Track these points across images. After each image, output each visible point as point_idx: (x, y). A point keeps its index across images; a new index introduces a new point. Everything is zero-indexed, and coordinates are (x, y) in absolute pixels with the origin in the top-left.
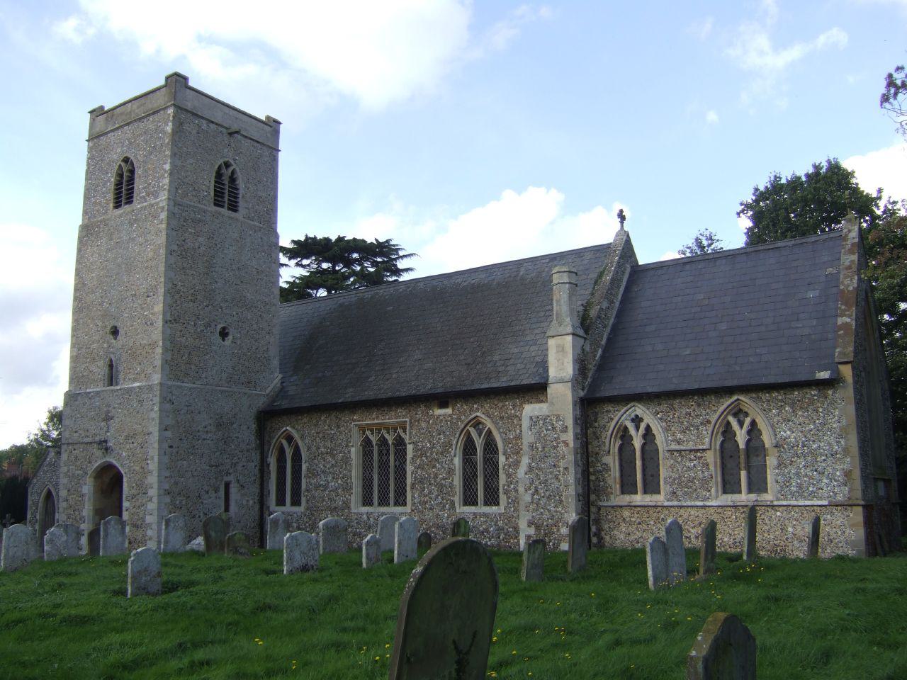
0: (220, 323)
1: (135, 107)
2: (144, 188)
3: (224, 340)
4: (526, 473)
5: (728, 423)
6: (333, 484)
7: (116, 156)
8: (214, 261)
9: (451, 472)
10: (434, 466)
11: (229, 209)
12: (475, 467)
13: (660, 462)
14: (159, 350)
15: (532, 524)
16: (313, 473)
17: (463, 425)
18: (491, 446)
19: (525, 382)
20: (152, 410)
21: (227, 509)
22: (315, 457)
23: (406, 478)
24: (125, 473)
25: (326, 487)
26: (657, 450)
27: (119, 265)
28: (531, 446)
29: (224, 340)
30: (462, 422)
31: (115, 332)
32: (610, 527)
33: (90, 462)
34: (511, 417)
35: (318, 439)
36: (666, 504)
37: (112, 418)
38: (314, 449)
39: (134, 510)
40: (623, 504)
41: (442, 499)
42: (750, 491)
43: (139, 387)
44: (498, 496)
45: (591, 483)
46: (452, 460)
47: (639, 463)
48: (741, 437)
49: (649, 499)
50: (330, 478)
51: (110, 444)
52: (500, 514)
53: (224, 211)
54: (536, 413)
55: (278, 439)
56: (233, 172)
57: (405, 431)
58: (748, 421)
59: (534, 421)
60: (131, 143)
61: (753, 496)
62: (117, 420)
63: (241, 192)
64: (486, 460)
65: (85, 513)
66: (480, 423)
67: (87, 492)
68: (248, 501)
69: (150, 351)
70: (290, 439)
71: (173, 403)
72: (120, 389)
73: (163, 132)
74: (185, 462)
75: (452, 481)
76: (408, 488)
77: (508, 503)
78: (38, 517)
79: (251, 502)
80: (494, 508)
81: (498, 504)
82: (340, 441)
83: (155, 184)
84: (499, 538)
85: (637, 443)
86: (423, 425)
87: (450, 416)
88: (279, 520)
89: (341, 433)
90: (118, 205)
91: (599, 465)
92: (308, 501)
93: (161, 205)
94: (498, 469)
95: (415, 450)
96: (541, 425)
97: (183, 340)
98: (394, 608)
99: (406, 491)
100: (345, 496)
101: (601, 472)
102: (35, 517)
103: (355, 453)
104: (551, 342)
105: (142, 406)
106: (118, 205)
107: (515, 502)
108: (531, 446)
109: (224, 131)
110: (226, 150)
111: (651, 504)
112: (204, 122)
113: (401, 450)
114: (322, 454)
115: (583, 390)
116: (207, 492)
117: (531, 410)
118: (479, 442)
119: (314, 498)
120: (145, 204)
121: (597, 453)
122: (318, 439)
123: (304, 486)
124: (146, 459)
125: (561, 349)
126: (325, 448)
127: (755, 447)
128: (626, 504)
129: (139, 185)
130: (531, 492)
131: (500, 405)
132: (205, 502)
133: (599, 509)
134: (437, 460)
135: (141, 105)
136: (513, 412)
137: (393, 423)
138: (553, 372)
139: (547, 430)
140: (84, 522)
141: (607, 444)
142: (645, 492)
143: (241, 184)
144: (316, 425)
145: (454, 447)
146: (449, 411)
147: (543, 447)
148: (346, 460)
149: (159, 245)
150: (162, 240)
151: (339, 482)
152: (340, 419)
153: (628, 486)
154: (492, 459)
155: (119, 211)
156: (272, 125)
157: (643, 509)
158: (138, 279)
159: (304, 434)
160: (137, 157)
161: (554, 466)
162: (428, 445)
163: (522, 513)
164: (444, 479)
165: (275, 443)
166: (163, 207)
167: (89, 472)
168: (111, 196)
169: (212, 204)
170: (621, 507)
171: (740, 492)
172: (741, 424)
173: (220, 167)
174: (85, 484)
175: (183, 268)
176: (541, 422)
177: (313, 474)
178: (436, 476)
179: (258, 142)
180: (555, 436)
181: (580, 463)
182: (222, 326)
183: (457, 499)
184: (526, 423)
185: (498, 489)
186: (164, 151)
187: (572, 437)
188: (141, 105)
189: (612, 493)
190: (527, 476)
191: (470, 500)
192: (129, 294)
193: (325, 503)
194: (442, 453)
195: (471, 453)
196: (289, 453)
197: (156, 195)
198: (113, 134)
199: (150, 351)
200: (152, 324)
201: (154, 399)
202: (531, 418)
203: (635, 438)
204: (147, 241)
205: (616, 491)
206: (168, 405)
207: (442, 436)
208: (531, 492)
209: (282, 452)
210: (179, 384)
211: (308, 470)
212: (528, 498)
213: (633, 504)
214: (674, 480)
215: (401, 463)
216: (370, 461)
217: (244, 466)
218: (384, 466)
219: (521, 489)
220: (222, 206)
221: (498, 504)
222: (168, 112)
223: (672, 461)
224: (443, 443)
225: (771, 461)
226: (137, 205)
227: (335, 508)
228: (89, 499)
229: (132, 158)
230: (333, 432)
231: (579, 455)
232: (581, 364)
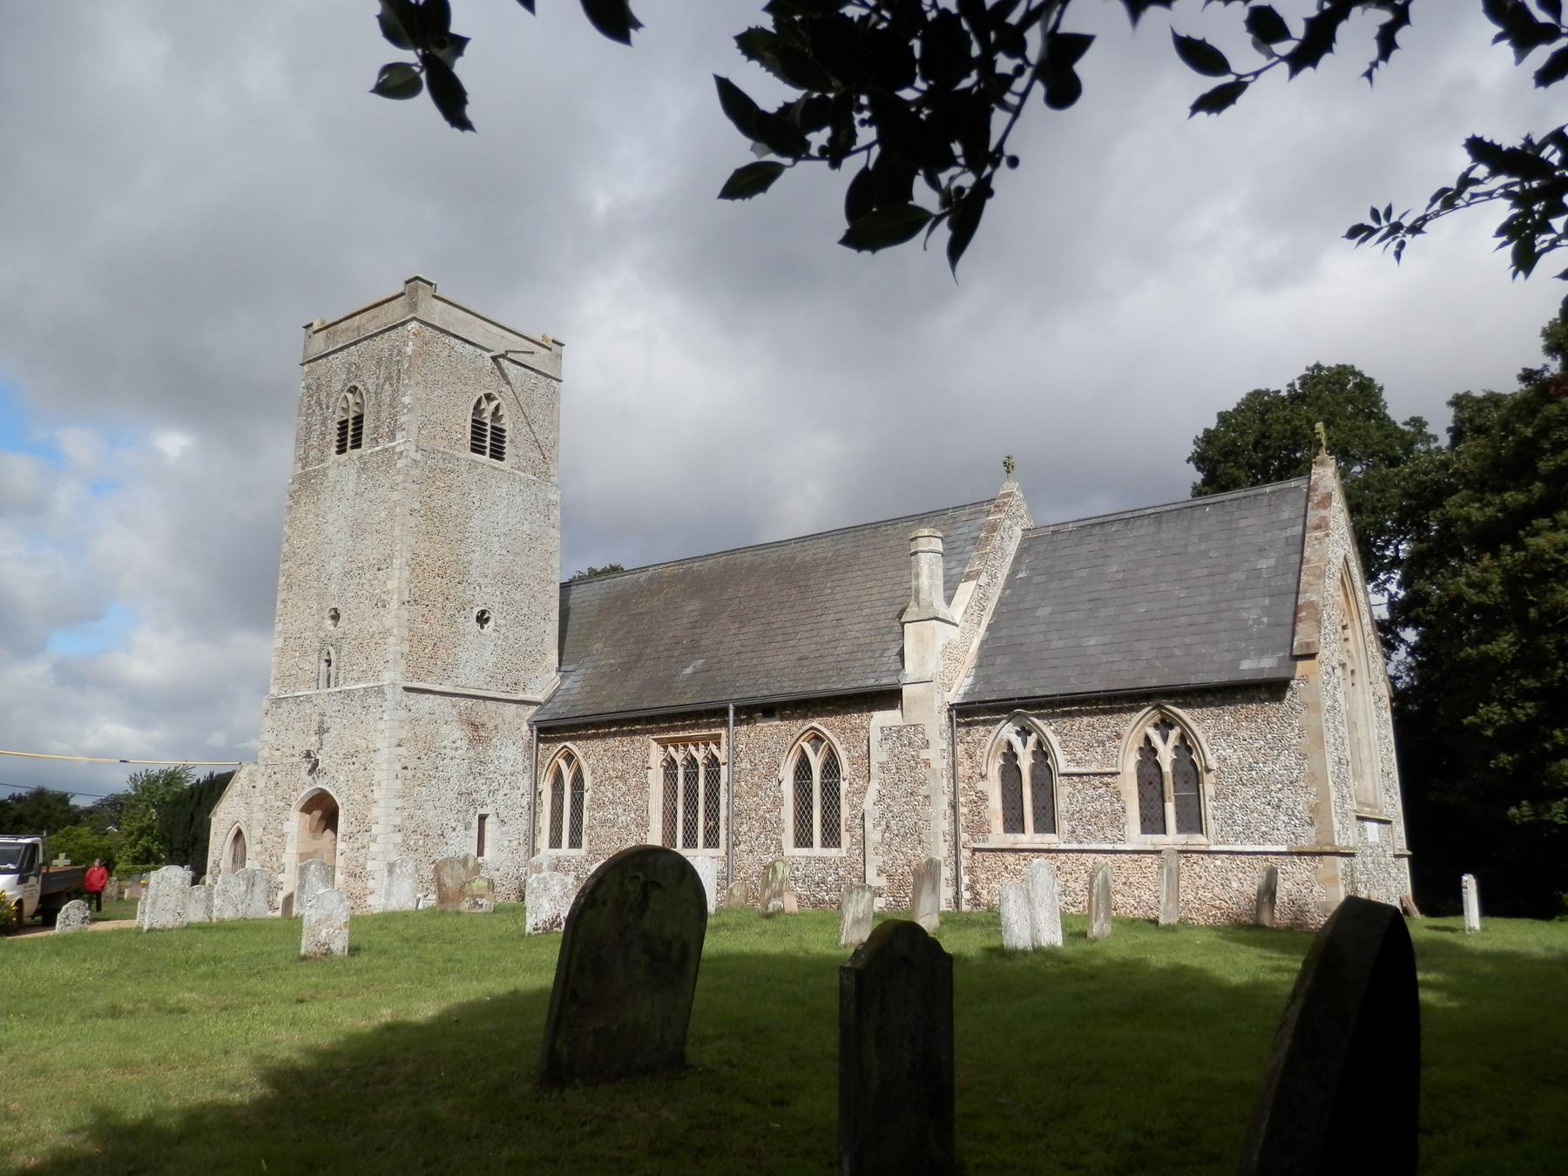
1: (364, 321)
5: (1147, 739)
6: (624, 818)
9: (778, 803)
28: (883, 767)
31: (336, 617)
48: (1166, 755)
53: (485, 459)
58: (1032, 739)
61: (1183, 838)
83: (390, 423)
85: (1025, 762)
90: (341, 450)
94: (839, 798)
97: (426, 626)
103: (656, 778)
106: (339, 453)
108: (883, 767)
117: (881, 719)
118: (816, 763)
127: (1190, 772)
148: (643, 786)
155: (344, 456)
159: (590, 754)
171: (1164, 832)
172: (1165, 738)
173: (479, 402)
179: (532, 369)
183: (788, 836)
184: (875, 736)
191: (803, 839)
209: (558, 777)
213: (1018, 846)
218: (691, 778)
219: (869, 825)
225: (1209, 788)
230: (625, 749)
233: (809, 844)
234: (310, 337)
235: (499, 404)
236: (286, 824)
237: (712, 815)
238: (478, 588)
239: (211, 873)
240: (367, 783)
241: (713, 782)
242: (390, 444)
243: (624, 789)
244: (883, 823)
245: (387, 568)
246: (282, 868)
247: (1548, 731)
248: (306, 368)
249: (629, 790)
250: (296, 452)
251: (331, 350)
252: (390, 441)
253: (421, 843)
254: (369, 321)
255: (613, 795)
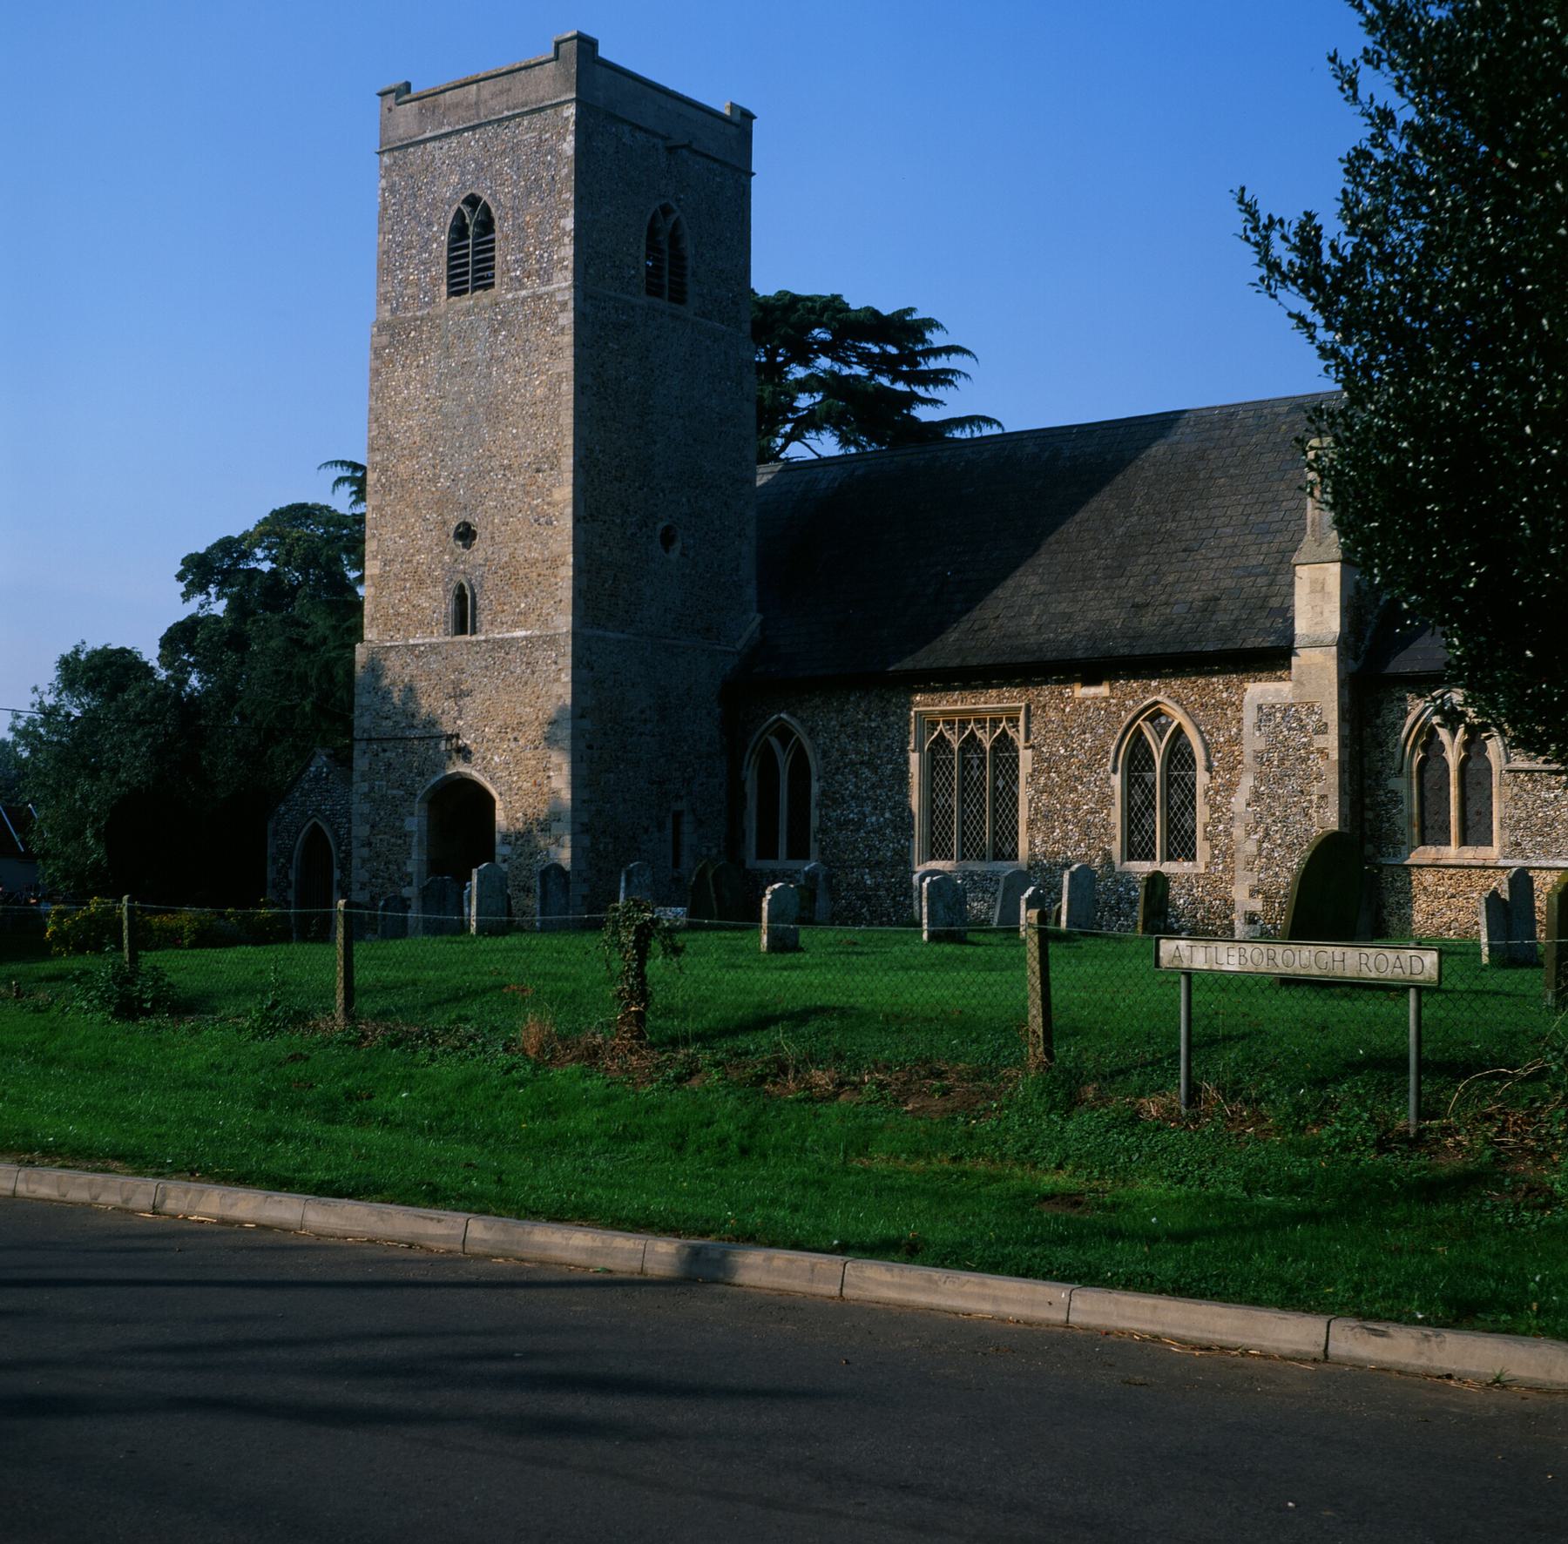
0: (662, 519)
1: (485, 94)
2: (516, 261)
3: (667, 551)
4: (1248, 805)
6: (874, 819)
7: (449, 192)
8: (651, 402)
10: (1075, 789)
11: (671, 299)
12: (1150, 791)
13: (1494, 790)
14: (567, 572)
15: (1258, 892)
16: (831, 798)
17: (1130, 717)
18: (1183, 755)
19: (1248, 645)
20: (557, 680)
21: (676, 863)
22: (838, 768)
23: (1017, 811)
24: (500, 794)
25: (860, 825)
26: (1490, 769)
27: (469, 408)
28: (1258, 757)
29: (667, 551)
30: (1128, 710)
31: (466, 534)
32: (1398, 903)
33: (421, 774)
34: (1222, 705)
35: (843, 736)
36: (1502, 863)
37: (469, 693)
38: (836, 755)
39: (521, 860)
40: (1424, 863)
41: (1089, 847)
42: (1464, 841)
43: (526, 638)
44: (1194, 844)
45: (1367, 824)
46: (1109, 778)
47: (1454, 791)
49: (1471, 854)
50: (868, 810)
51: (464, 741)
52: (1197, 875)
53: (662, 303)
54: (1271, 700)
55: (763, 734)
56: (676, 225)
57: (1016, 726)
59: (1265, 713)
60: (480, 168)
62: (479, 697)
63: (690, 263)
64: (1169, 782)
65: (411, 868)
66: (1162, 714)
67: (414, 828)
68: (709, 849)
69: (547, 572)
70: (784, 734)
71: (592, 669)
72: (485, 641)
73: (558, 155)
74: (612, 775)
75: (1108, 815)
76: (1022, 828)
77: (1213, 856)
78: (292, 877)
79: (715, 851)
80: (1186, 864)
81: (1192, 857)
82: (888, 742)
83: (542, 256)
84: (1195, 917)
86: (1052, 714)
87: (1106, 699)
88: (817, 875)
89: (889, 727)
90: (456, 289)
91: (1382, 792)
92: (822, 850)
93: (559, 298)
94: (1194, 797)
95: (1039, 758)
96: (1278, 720)
97: (605, 551)
98: (504, 1177)
99: (1017, 833)
100: (899, 842)
101: (1385, 805)
102: (286, 876)
104: (1302, 572)
105: (533, 673)
106: (456, 289)
107: (1228, 854)
108: (1258, 757)
109: (660, 143)
110: (664, 182)
111: (1474, 862)
112: (627, 128)
113: (1007, 760)
114: (852, 763)
115: (1356, 659)
116: (646, 830)
117: (1260, 691)
119: (836, 844)
120: (524, 293)
121: (1380, 773)
122: (843, 736)
123: (815, 823)
124: (546, 769)
125: (1319, 588)
126: (857, 754)
128: (1430, 862)
129: (504, 255)
130: (1256, 837)
131: (1201, 681)
132: (643, 847)
133: (1381, 871)
134: (1079, 779)
135: (501, 92)
136: (1225, 695)
137: (994, 710)
138: (1301, 627)
139: (1290, 729)
140: (410, 884)
141: (1398, 756)
142: (1464, 841)
143: (688, 247)
144: (841, 711)
145: (1112, 755)
146: (1103, 690)
147: (1282, 760)
149: (559, 374)
150: (566, 364)
151: (887, 815)
152: (889, 701)
153: (1433, 833)
154: (1183, 778)
156: (743, 120)
157: (1461, 872)
158: (515, 437)
160: (499, 197)
161: (1302, 792)
162: (1062, 751)
163: (1240, 873)
164: (1092, 813)
165: (756, 744)
166: (565, 303)
167: (420, 793)
168: (440, 270)
169: (643, 293)
170: (1420, 866)
173: (654, 218)
174: (412, 814)
175: (603, 418)
176: (1278, 715)
177: (834, 801)
178: (1077, 808)
179: (715, 160)
180: (1305, 740)
181: (1348, 788)
182: (665, 524)
184: (1249, 716)
185: (1194, 832)
186: (560, 193)
187: (1336, 744)
188: (501, 92)
189: (1404, 843)
190: (1250, 809)
192: (495, 463)
193: (857, 853)
194: (1089, 767)
195: (1143, 768)
196: (784, 762)
197: (546, 276)
198: (437, 144)
199: (547, 572)
200: (549, 523)
201: (560, 660)
202: (1260, 708)
203: (1448, 748)
204: (531, 365)
205: (1412, 838)
206: (584, 671)
207: (1088, 735)
208: (1256, 837)
210: (600, 632)
211: (823, 793)
212: (1251, 847)
213: (1442, 862)
214: (1519, 821)
215: (1007, 783)
216: (947, 779)
217: (702, 785)
219: (1238, 832)
220: (659, 295)
221: (1194, 858)
222: (565, 115)
223: (1516, 790)
224: (1090, 747)
226: (501, 291)
227: (878, 863)
228: (420, 842)
229: (485, 198)
230: (873, 725)
231: (1347, 776)
232: (1355, 607)
233: (775, 856)
234: (390, 110)
235: (678, 218)
236: (408, 820)
237: (1007, 816)
238: (661, 495)
239: (274, 887)
240: (541, 767)
241: (1007, 771)
242: (544, 289)
243: (875, 779)
244: (1261, 830)
245: (551, 469)
246: (408, 879)
247: (1517, 52)
248: (386, 159)
249: (881, 781)
250: (378, 286)
251: (428, 135)
252: (543, 284)
253: (610, 847)
254: (494, 96)
255: (856, 786)
